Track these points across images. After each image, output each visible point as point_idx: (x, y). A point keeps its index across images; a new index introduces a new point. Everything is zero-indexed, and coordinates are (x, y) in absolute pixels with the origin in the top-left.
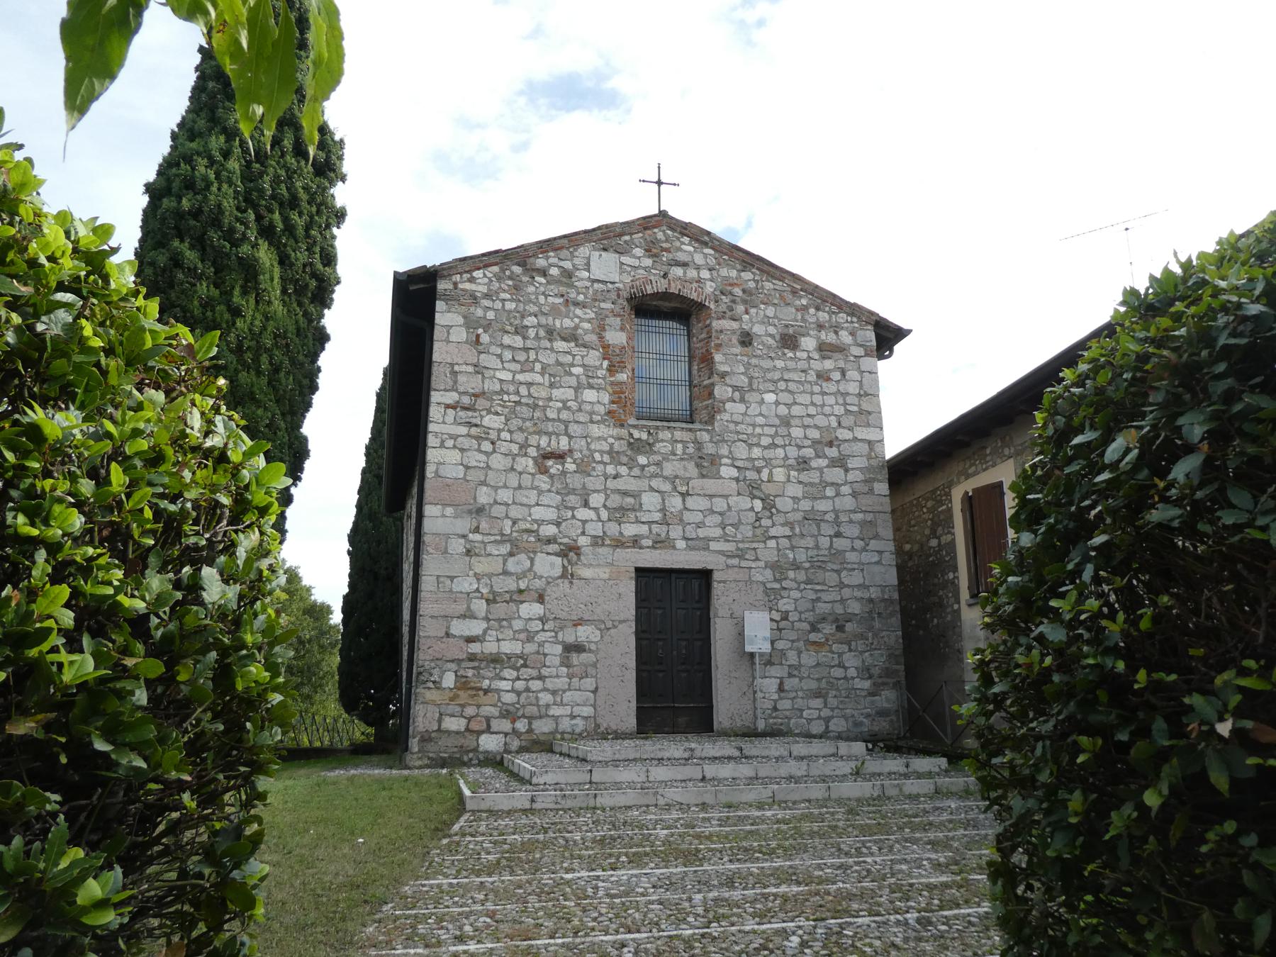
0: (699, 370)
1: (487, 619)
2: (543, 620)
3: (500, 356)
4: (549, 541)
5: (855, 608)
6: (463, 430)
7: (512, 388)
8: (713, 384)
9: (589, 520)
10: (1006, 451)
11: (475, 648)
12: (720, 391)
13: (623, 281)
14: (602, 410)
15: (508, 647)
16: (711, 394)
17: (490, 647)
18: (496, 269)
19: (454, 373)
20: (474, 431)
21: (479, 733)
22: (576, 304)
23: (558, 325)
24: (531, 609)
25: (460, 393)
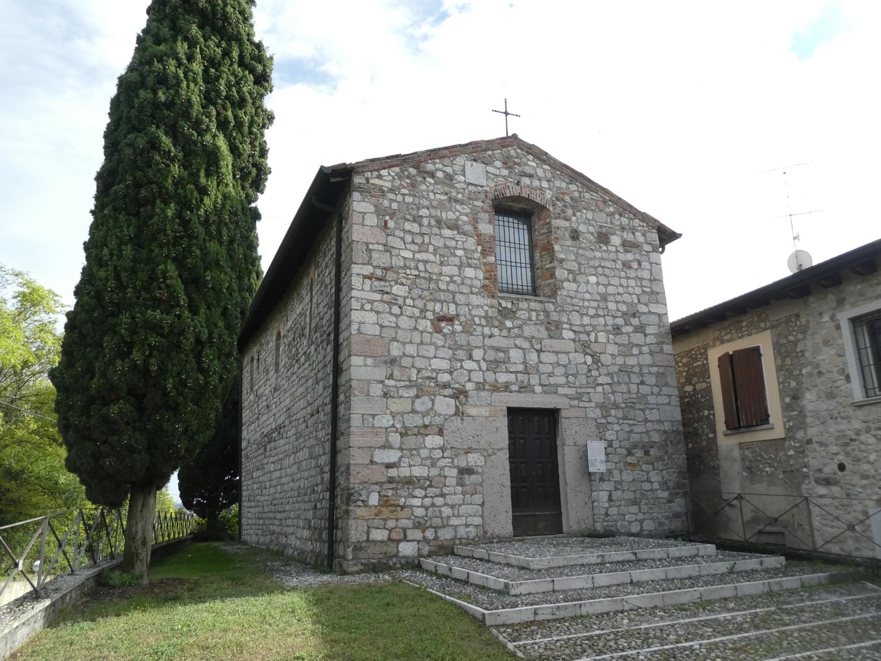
0: (541, 256)
1: (401, 449)
2: (443, 449)
3: (403, 239)
4: (445, 386)
5: (656, 437)
6: (378, 297)
8: (554, 268)
9: (473, 370)
10: (762, 325)
11: (393, 472)
12: (560, 273)
13: (489, 185)
14: (478, 284)
16: (552, 275)
17: (404, 472)
18: (397, 169)
19: (369, 251)
24: (434, 441)
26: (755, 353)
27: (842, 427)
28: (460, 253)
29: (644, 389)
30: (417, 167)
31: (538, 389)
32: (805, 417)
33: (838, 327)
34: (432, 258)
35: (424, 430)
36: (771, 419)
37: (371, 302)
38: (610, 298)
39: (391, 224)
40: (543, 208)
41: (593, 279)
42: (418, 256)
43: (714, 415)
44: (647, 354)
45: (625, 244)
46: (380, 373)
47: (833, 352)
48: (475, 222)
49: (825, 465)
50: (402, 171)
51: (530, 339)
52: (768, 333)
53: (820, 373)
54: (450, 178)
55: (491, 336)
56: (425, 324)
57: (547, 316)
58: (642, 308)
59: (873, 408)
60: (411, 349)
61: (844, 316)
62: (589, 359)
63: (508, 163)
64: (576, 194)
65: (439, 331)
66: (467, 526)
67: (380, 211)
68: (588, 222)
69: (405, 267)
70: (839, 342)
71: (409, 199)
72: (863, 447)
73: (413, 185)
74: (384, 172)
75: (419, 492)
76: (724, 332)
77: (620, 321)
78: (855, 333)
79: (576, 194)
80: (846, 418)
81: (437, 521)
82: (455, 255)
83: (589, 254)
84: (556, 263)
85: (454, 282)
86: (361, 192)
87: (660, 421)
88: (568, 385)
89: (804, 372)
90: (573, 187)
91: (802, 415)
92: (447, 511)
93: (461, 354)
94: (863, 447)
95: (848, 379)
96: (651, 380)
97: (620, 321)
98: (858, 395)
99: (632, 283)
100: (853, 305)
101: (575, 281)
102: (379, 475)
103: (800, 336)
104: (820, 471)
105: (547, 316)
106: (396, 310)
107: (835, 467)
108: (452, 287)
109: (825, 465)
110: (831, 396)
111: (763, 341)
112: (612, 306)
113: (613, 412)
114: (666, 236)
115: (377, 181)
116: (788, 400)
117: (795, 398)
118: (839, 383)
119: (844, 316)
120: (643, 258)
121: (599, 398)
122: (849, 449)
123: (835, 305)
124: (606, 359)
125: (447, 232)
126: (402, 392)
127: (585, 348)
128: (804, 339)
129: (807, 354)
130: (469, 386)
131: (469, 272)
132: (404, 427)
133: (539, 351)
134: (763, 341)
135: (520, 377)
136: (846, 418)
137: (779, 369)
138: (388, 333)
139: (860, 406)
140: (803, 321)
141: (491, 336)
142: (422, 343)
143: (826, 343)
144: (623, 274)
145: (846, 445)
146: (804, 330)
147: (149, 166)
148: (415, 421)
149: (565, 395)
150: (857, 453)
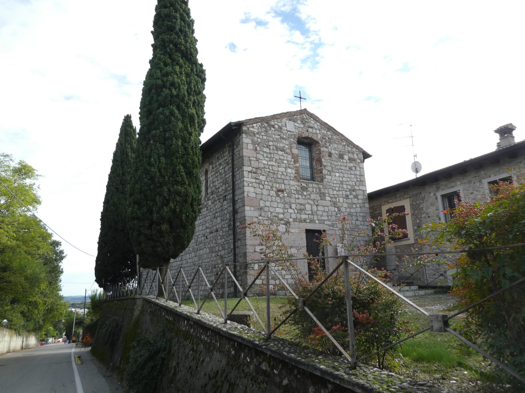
3: (263, 155)
4: (282, 220)
6: (254, 180)
8: (322, 169)
10: (406, 196)
12: (325, 172)
13: (296, 131)
14: (293, 175)
16: (321, 172)
18: (260, 124)
19: (250, 160)
22: (283, 139)
25: (253, 168)
28: (285, 162)
29: (358, 223)
31: (317, 222)
33: (437, 198)
34: (275, 164)
37: (252, 183)
39: (258, 148)
40: (317, 142)
41: (337, 174)
42: (269, 163)
44: (360, 207)
45: (350, 159)
46: (256, 214)
47: (434, 208)
48: (291, 148)
50: (262, 125)
51: (313, 200)
52: (408, 200)
53: (429, 217)
54: (280, 128)
56: (273, 193)
57: (320, 190)
60: (268, 204)
61: (439, 194)
63: (303, 122)
64: (330, 136)
65: (278, 196)
67: (254, 143)
68: (335, 149)
69: (264, 168)
70: (437, 204)
71: (265, 137)
73: (266, 131)
74: (255, 125)
76: (389, 199)
77: (348, 193)
78: (443, 201)
79: (330, 136)
82: (283, 163)
83: (336, 163)
84: (323, 167)
85: (284, 175)
86: (246, 134)
90: (329, 133)
93: (287, 206)
96: (360, 219)
97: (348, 193)
99: (353, 176)
100: (443, 190)
101: (330, 175)
103: (421, 201)
105: (320, 190)
106: (261, 187)
108: (283, 177)
111: (406, 203)
112: (345, 186)
114: (366, 156)
115: (252, 129)
116: (416, 228)
117: (419, 227)
118: (437, 221)
119: (439, 194)
120: (357, 166)
124: (343, 209)
125: (280, 153)
128: (423, 202)
129: (424, 209)
130: (291, 220)
131: (289, 170)
133: (317, 205)
134: (406, 203)
135: (310, 216)
138: (259, 197)
140: (423, 195)
141: (298, 199)
142: (272, 201)
143: (432, 205)
147: (170, 123)
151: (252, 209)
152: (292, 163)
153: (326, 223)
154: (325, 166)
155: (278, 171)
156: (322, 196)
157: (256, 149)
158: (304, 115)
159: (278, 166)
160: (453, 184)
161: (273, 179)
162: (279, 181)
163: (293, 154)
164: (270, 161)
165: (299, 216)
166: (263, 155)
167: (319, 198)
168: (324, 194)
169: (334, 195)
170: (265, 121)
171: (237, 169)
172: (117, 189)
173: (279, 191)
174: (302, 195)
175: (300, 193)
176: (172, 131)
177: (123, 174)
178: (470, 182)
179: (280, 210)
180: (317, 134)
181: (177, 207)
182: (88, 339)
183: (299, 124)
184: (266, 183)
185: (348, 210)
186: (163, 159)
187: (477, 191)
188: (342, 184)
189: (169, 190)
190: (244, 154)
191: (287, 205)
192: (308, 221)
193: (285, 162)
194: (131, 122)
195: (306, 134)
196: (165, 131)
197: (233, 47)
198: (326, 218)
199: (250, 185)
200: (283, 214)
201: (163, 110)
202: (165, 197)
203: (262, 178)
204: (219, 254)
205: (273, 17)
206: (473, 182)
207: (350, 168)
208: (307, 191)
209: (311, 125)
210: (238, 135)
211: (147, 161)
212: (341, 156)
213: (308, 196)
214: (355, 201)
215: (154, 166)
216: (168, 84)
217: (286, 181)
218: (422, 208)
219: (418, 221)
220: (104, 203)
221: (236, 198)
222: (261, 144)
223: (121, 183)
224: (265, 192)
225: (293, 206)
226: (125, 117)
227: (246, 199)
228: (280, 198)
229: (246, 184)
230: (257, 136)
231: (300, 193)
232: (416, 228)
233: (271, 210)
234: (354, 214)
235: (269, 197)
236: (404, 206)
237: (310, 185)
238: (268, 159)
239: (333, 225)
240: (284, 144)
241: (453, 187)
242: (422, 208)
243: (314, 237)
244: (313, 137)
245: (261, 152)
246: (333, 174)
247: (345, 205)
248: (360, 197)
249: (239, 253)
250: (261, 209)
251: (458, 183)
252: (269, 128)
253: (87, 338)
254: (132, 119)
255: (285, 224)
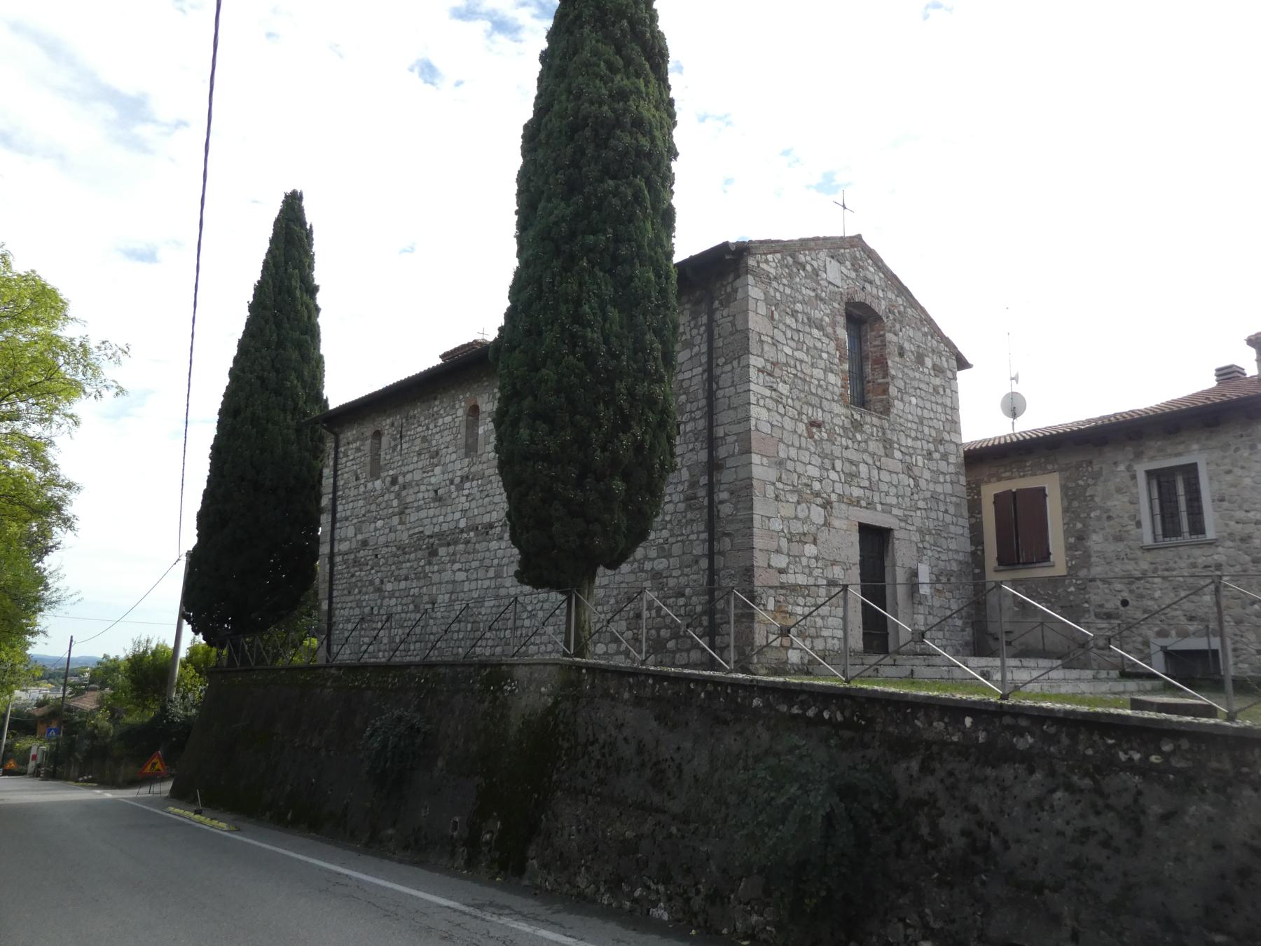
0: (873, 369)
1: (789, 555)
2: (817, 558)
3: (784, 333)
4: (818, 495)
5: (955, 567)
6: (767, 392)
7: (792, 363)
8: (888, 384)
9: (834, 483)
10: (1050, 467)
11: (784, 578)
12: (893, 391)
13: (843, 286)
14: (837, 391)
15: (801, 580)
16: (886, 391)
17: (790, 579)
18: (779, 256)
19: (762, 342)
20: (774, 395)
21: (787, 648)
22: (821, 300)
23: (63, 369)
24: (810, 550)
25: (767, 360)
26: (1041, 493)
27: (1129, 567)
28: (825, 356)
29: (948, 519)
30: (793, 256)
31: (879, 507)
32: (1090, 556)
33: (1134, 477)
34: (805, 358)
35: (802, 539)
36: (1052, 558)
37: (764, 397)
38: (925, 422)
39: (776, 316)
40: (879, 318)
41: (914, 400)
42: (796, 354)
43: (983, 551)
44: (948, 481)
45: (935, 367)
46: (772, 474)
47: (1126, 499)
48: (834, 324)
49: (1107, 601)
50: (783, 259)
51: (873, 455)
52: (1056, 475)
53: (1109, 518)
54: (816, 272)
55: (847, 448)
56: (802, 428)
57: (884, 434)
58: (946, 437)
59: (1162, 552)
60: (793, 453)
61: (1141, 469)
62: (912, 482)
63: (856, 267)
64: (902, 309)
65: (811, 436)
66: (833, 638)
67: (768, 301)
68: (910, 339)
69: (787, 364)
70: (1134, 491)
71: (788, 291)
72: (1148, 586)
73: (791, 276)
74: (770, 257)
75: (801, 601)
76: (1002, 470)
77: (931, 446)
78: (1149, 483)
79: (902, 309)
80: (1134, 559)
81: (812, 631)
82: (821, 357)
83: (911, 374)
84: (889, 380)
85: (821, 386)
86: (754, 276)
87: (957, 552)
88: (899, 506)
89: (1092, 515)
90: (900, 301)
91: (1087, 555)
92: (819, 622)
93: (827, 463)
94: (1148, 586)
95: (1139, 524)
96: (952, 510)
97: (931, 446)
98: (1148, 540)
99: (940, 409)
100: (1152, 459)
101: (902, 400)
102: (775, 580)
103: (1091, 481)
104: (1101, 606)
105: (884, 434)
106: (781, 410)
107: (1119, 603)
108: (820, 392)
109: (1107, 601)
110: (1118, 538)
111: (1051, 483)
112: (926, 430)
113: (927, 537)
114: (963, 364)
115: (764, 266)
116: (1072, 540)
117: (1081, 538)
118: (1129, 528)
119: (1141, 469)
120: (947, 385)
121: (918, 522)
122: (1134, 587)
123: (1132, 456)
124: (923, 484)
125: (816, 332)
126: (789, 496)
127: (909, 469)
128: (1095, 484)
129: (1097, 499)
130: (834, 497)
131: (832, 378)
132: (790, 533)
133: (879, 469)
134: (1051, 483)
135: (868, 493)
136: (1134, 559)
137: (1066, 510)
138: (777, 433)
139: (1149, 550)
140: (1096, 468)
141: (847, 448)
142: (800, 448)
143: (1119, 490)
144: (933, 399)
145: (1131, 583)
146: (1096, 476)
147: (630, 221)
148: (797, 527)
149: (896, 516)
150: (1141, 590)
151: (765, 461)
152: (836, 361)
153: (895, 511)
154: (893, 377)
155: (812, 377)
156: (888, 444)
157: (772, 318)
158: (852, 249)
159: (812, 365)
160: (1181, 448)
161: (802, 395)
162: (815, 400)
163: (837, 339)
164: (797, 349)
165: (847, 490)
166: (784, 333)
167: (881, 452)
168: (891, 442)
169: (907, 447)
170: (792, 252)
171: (721, 361)
172: (263, 380)
173: (813, 424)
174: (853, 439)
175: (850, 435)
176: (633, 243)
177: (280, 344)
178: (1225, 447)
179: (813, 471)
180: (881, 302)
181: (647, 437)
182: (158, 766)
183: (847, 269)
184: (790, 401)
185: (931, 486)
186: (613, 313)
187: (1243, 468)
188: (922, 423)
189: (631, 393)
190: (751, 325)
191: (826, 461)
192: (863, 503)
193: (825, 356)
194: (301, 210)
195: (859, 297)
196: (617, 240)
197: (428, 71)
198: (894, 501)
199: (762, 402)
200: (821, 481)
201: (617, 187)
202: (621, 408)
203: (783, 388)
204: (648, 566)
205: (534, 16)
206: (1233, 448)
207: (935, 389)
208: (862, 432)
209: (870, 276)
210: (731, 278)
211: (568, 311)
212: (920, 360)
213: (863, 445)
214: (943, 466)
215: (591, 326)
216: (628, 119)
217: (825, 403)
218: (1092, 496)
219: (1079, 526)
220: (220, 413)
221: (720, 432)
222: (782, 307)
223: (273, 366)
224: (788, 424)
225: (838, 464)
226: (286, 197)
227: (754, 435)
228: (815, 441)
229: (753, 399)
230: (775, 284)
231: (850, 435)
232: (1072, 540)
233: (800, 468)
234: (942, 497)
235: (796, 436)
236: (1043, 489)
237: (868, 419)
238: (793, 344)
239: (905, 519)
240: (821, 313)
241: (1180, 454)
242: (1092, 496)
243: (875, 540)
244: (873, 306)
245: (781, 326)
246: (906, 398)
247: (927, 475)
248: (952, 459)
249: (725, 567)
250: (781, 463)
251: (1195, 447)
252: (795, 270)
253: (154, 764)
254: (304, 203)
255: (824, 506)
